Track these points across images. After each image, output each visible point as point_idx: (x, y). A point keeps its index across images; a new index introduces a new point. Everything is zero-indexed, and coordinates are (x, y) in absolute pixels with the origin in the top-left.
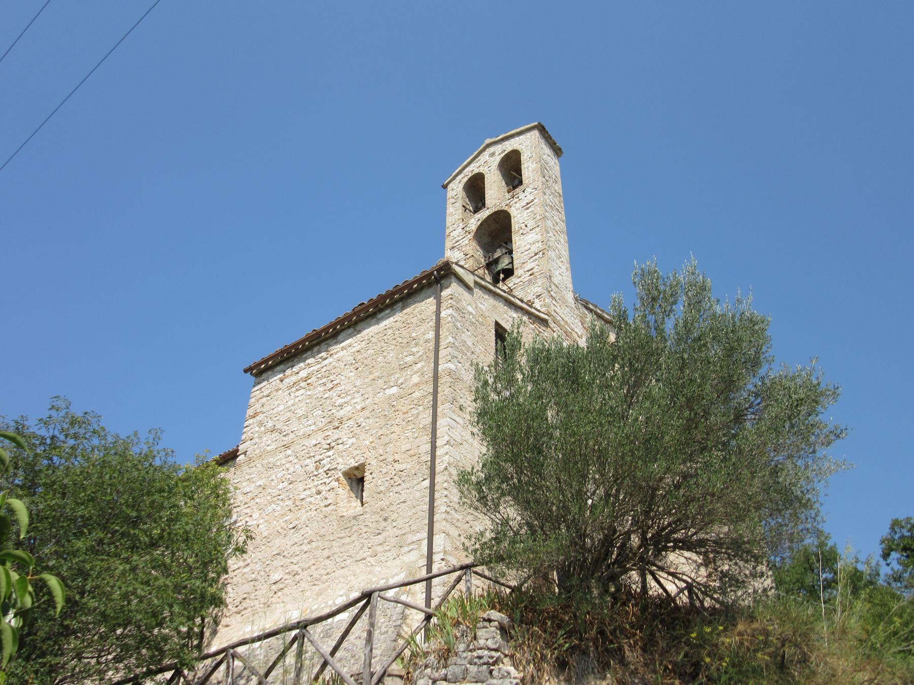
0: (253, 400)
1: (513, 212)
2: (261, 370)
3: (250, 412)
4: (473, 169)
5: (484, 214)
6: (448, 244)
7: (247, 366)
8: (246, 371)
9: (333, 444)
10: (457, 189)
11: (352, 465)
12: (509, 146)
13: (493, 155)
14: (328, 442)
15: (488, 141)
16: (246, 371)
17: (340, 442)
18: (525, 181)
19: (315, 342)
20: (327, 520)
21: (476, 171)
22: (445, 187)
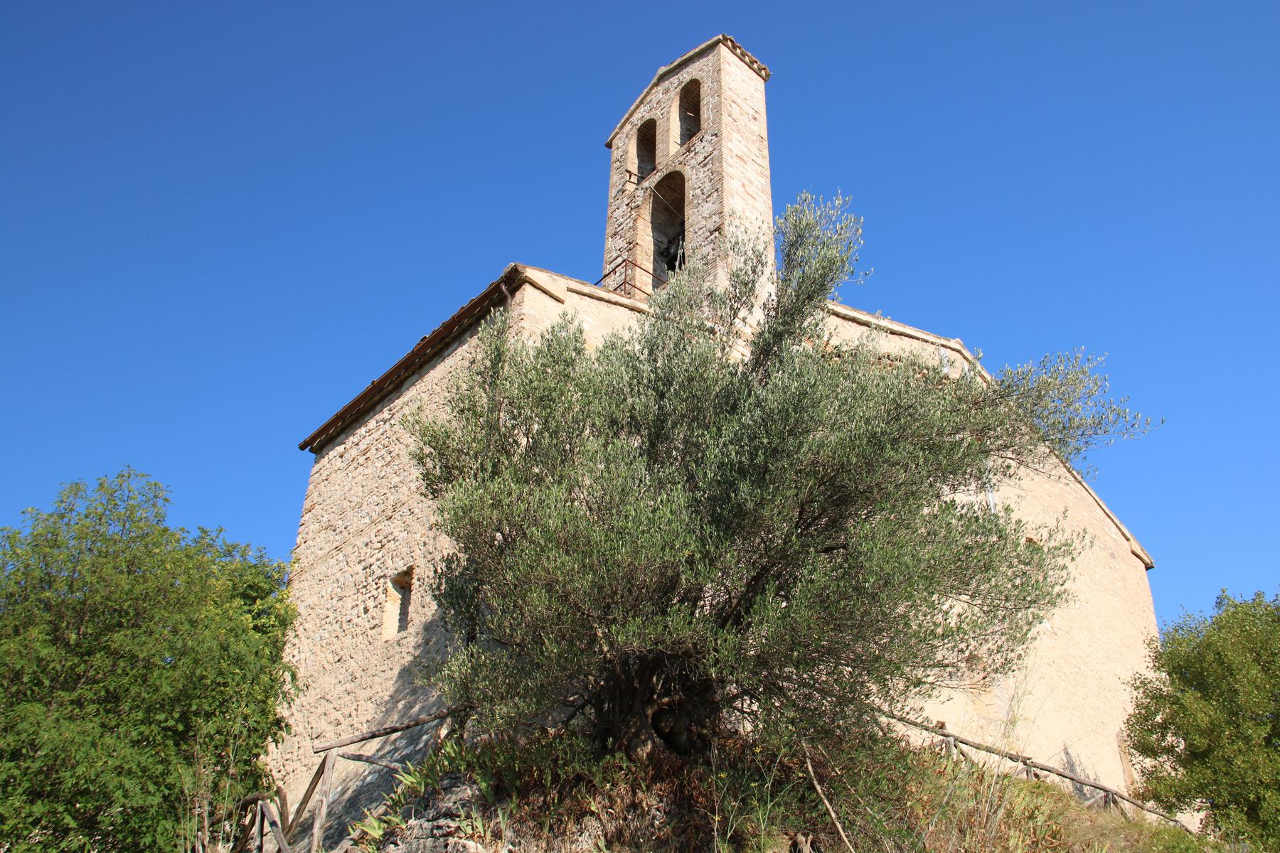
0: (311, 487)
1: (688, 172)
2: (320, 443)
3: (307, 505)
4: (640, 116)
5: (655, 178)
6: (610, 230)
7: (301, 441)
8: (302, 447)
9: (385, 541)
10: (627, 147)
11: (400, 570)
12: (686, 76)
13: (667, 91)
14: (380, 538)
15: (663, 69)
16: (302, 447)
17: (391, 538)
18: (704, 125)
19: (377, 398)
20: (1035, 394)
21: (647, 117)
22: (609, 146)
